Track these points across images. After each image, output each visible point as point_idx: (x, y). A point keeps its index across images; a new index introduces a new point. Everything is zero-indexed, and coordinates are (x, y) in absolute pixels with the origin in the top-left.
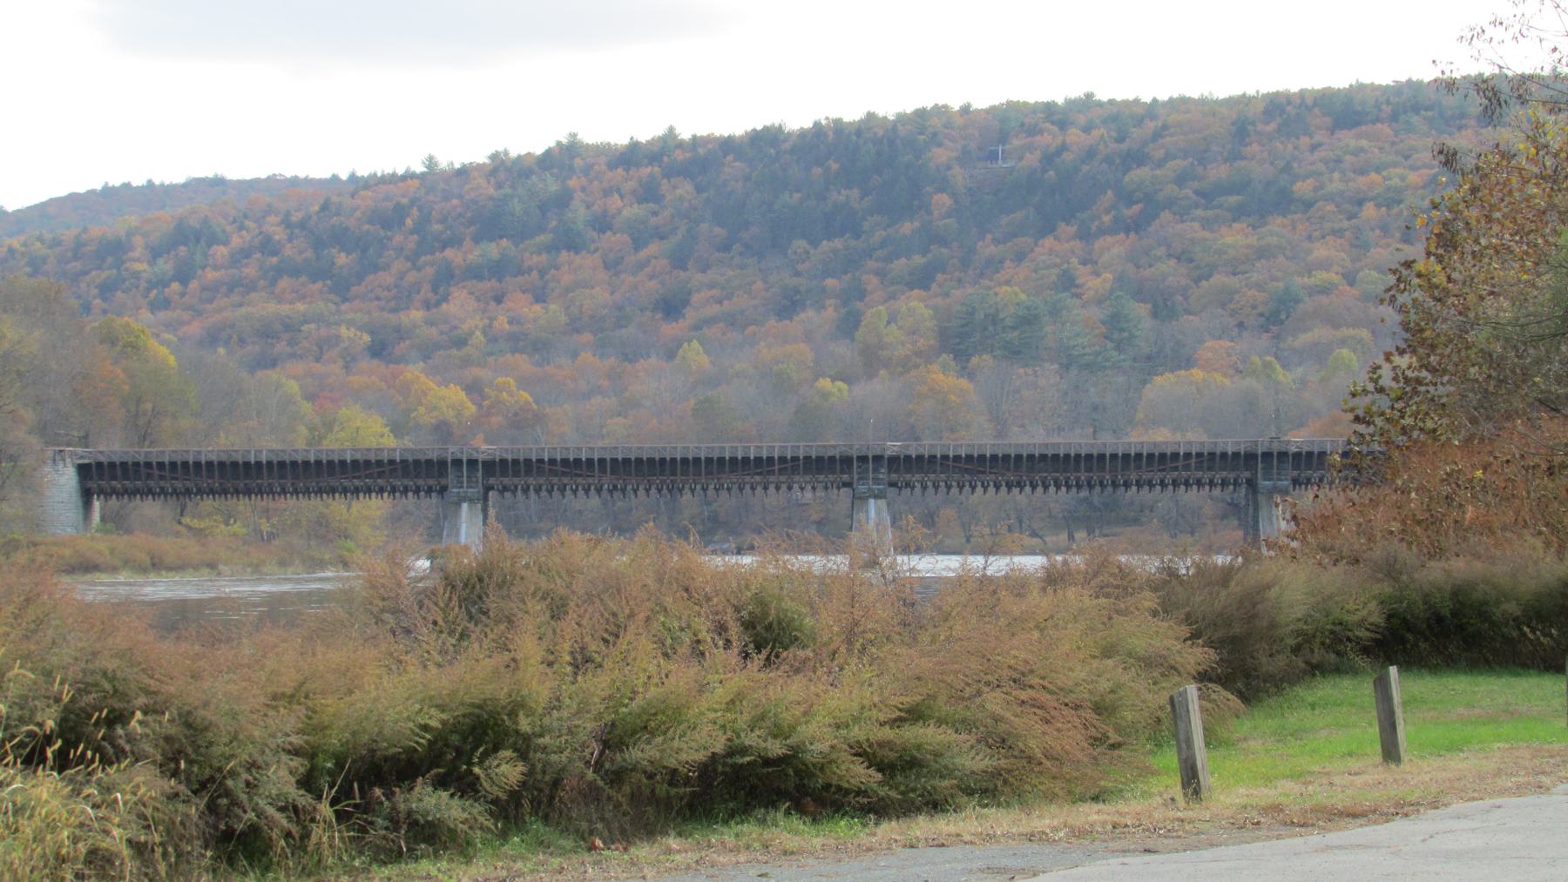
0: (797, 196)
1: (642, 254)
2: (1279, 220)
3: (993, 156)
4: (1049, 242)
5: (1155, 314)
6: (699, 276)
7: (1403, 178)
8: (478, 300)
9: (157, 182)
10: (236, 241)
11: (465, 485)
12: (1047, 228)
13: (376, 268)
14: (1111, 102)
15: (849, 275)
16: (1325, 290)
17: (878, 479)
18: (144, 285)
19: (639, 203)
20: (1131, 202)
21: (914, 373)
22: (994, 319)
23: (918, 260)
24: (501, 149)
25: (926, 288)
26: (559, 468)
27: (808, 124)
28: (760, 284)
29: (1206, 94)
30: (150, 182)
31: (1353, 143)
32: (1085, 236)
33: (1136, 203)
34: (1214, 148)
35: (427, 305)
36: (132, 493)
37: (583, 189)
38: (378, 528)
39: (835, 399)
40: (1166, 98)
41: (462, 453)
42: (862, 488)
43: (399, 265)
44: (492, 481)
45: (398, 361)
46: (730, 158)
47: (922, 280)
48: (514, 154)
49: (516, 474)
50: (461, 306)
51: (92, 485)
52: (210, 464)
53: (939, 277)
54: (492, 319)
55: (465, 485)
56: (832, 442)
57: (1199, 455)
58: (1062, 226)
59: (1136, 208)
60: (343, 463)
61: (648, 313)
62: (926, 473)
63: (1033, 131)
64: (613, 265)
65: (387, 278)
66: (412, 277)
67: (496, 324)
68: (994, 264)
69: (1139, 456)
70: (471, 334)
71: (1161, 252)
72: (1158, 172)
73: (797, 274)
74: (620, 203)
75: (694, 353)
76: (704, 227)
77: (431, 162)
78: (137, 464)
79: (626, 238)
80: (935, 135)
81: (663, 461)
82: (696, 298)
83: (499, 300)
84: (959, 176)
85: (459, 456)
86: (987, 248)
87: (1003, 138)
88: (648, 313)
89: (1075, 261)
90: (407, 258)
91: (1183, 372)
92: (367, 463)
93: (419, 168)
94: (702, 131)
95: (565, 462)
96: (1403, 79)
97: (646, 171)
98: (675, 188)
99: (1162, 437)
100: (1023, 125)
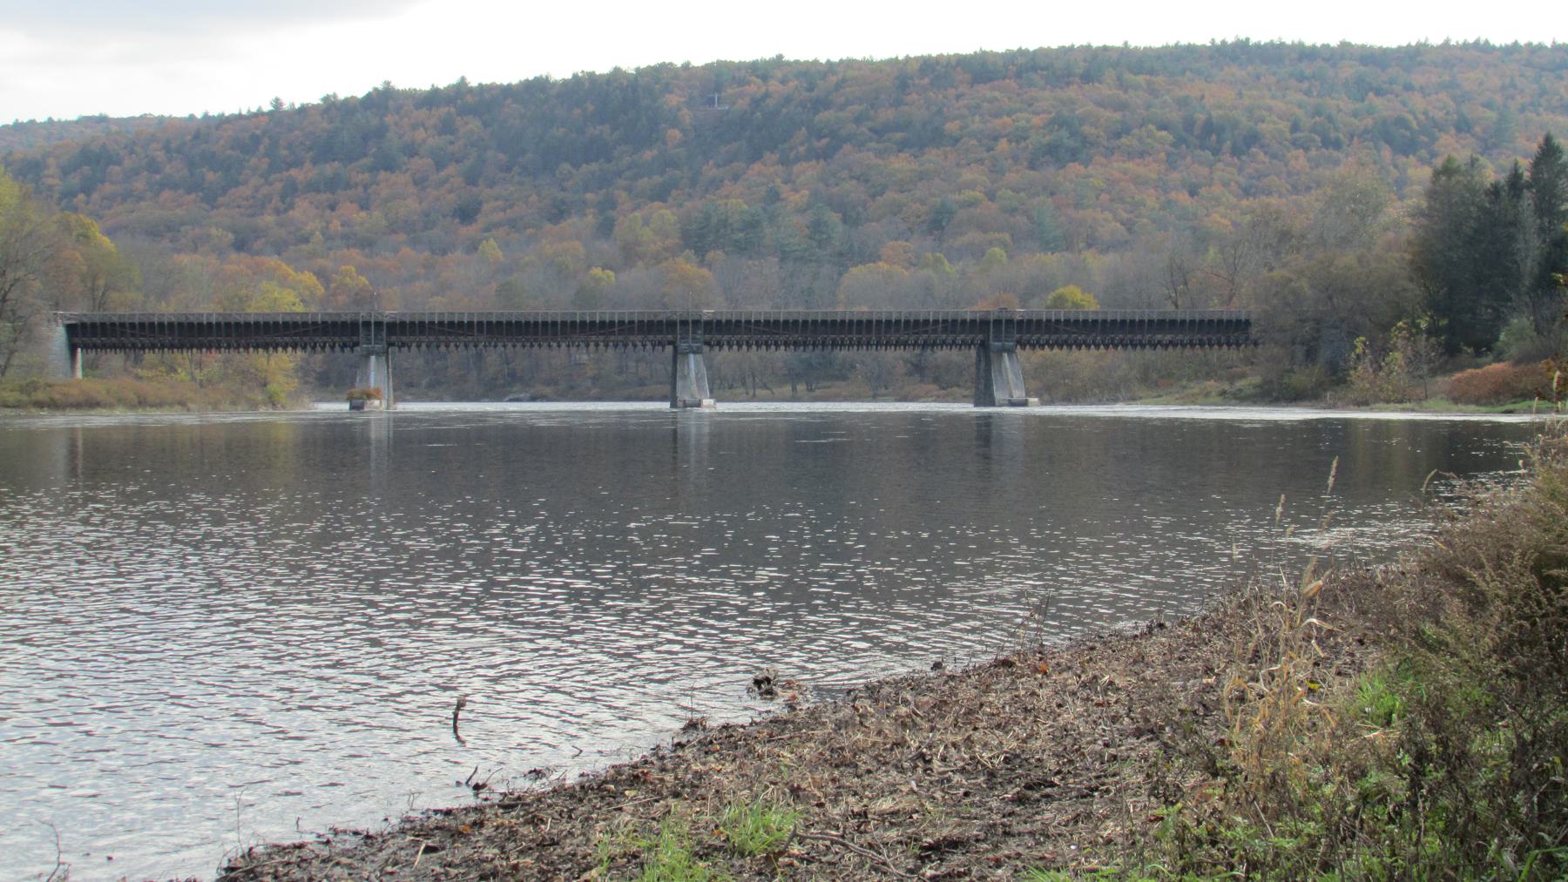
0: (562, 130)
1: (443, 174)
2: (934, 152)
3: (711, 102)
4: (757, 166)
5: (845, 221)
6: (488, 191)
7: (1028, 121)
8: (317, 208)
9: (56, 119)
10: (127, 163)
12: (756, 156)
13: (238, 184)
14: (797, 62)
15: (604, 191)
16: (971, 204)
18: (57, 195)
19: (440, 135)
20: (820, 137)
21: (664, 264)
22: (724, 223)
23: (657, 179)
24: (331, 93)
25: (665, 201)
27: (569, 76)
28: (534, 198)
29: (867, 57)
30: (50, 119)
31: (989, 94)
32: (785, 162)
33: (824, 137)
34: (883, 97)
35: (278, 212)
36: (104, 346)
37: (396, 124)
40: (792, 60)
43: (255, 181)
44: (393, 338)
45: (257, 254)
46: (509, 101)
47: (661, 195)
48: (341, 97)
49: (412, 333)
50: (303, 211)
51: (76, 340)
52: (171, 324)
53: (674, 192)
54: (328, 223)
56: (602, 313)
57: (945, 321)
58: (767, 155)
59: (825, 141)
60: (276, 324)
61: (449, 219)
62: (733, 334)
63: (742, 82)
64: (420, 182)
65: (246, 191)
66: (265, 190)
67: (331, 226)
68: (716, 184)
69: (898, 322)
70: (312, 234)
71: (845, 174)
72: (840, 114)
73: (563, 189)
74: (424, 135)
75: (492, 248)
76: (490, 153)
77: (277, 103)
78: (113, 324)
79: (430, 160)
80: (667, 84)
81: (527, 323)
82: (486, 207)
83: (332, 208)
84: (687, 116)
85: (367, 319)
86: (710, 171)
87: (718, 88)
88: (449, 219)
89: (778, 180)
90: (262, 176)
92: (295, 324)
93: (267, 108)
94: (486, 81)
95: (451, 324)
96: (1015, 48)
97: (444, 110)
98: (466, 123)
99: (861, 310)
100: (734, 78)
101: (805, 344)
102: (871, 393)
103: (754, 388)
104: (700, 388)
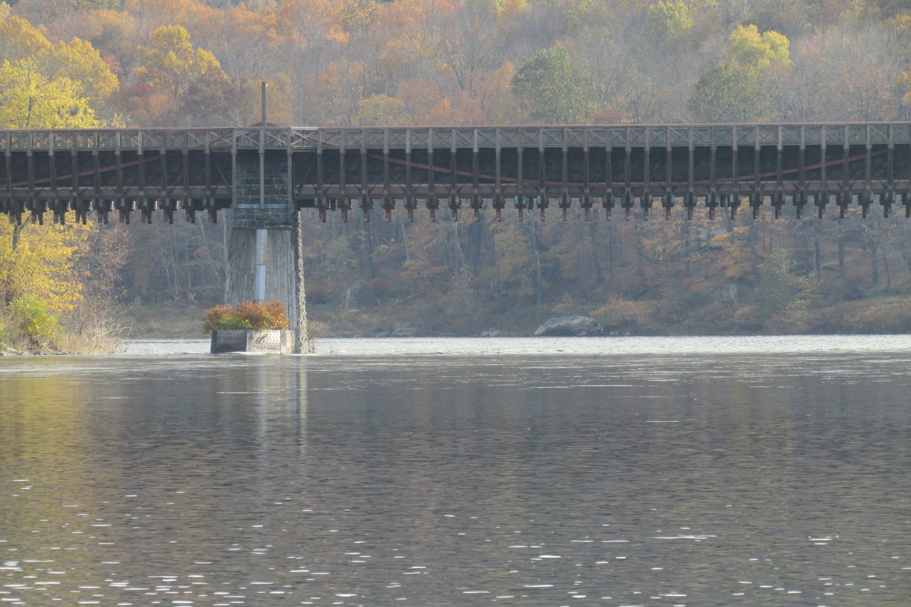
11: (262, 196)
26: (431, 167)
38: (66, 279)
39: (767, 62)
41: (257, 138)
44: (309, 189)
55: (262, 196)
81: (619, 152)
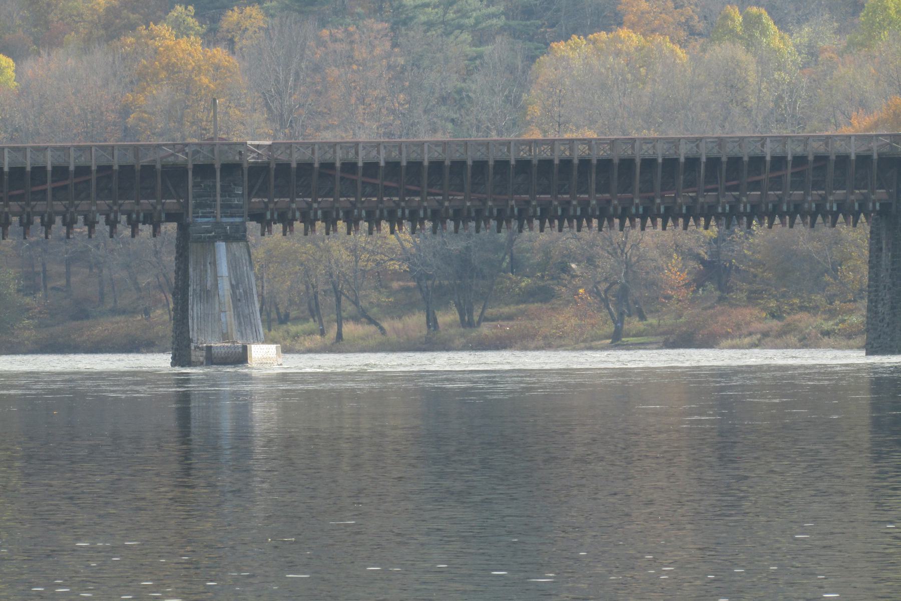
17: (230, 206)
42: (203, 222)
57: (800, 160)
69: (692, 162)
91: (603, 35)
101: (479, 216)
102: (610, 328)
103: (340, 322)
104: (244, 320)
